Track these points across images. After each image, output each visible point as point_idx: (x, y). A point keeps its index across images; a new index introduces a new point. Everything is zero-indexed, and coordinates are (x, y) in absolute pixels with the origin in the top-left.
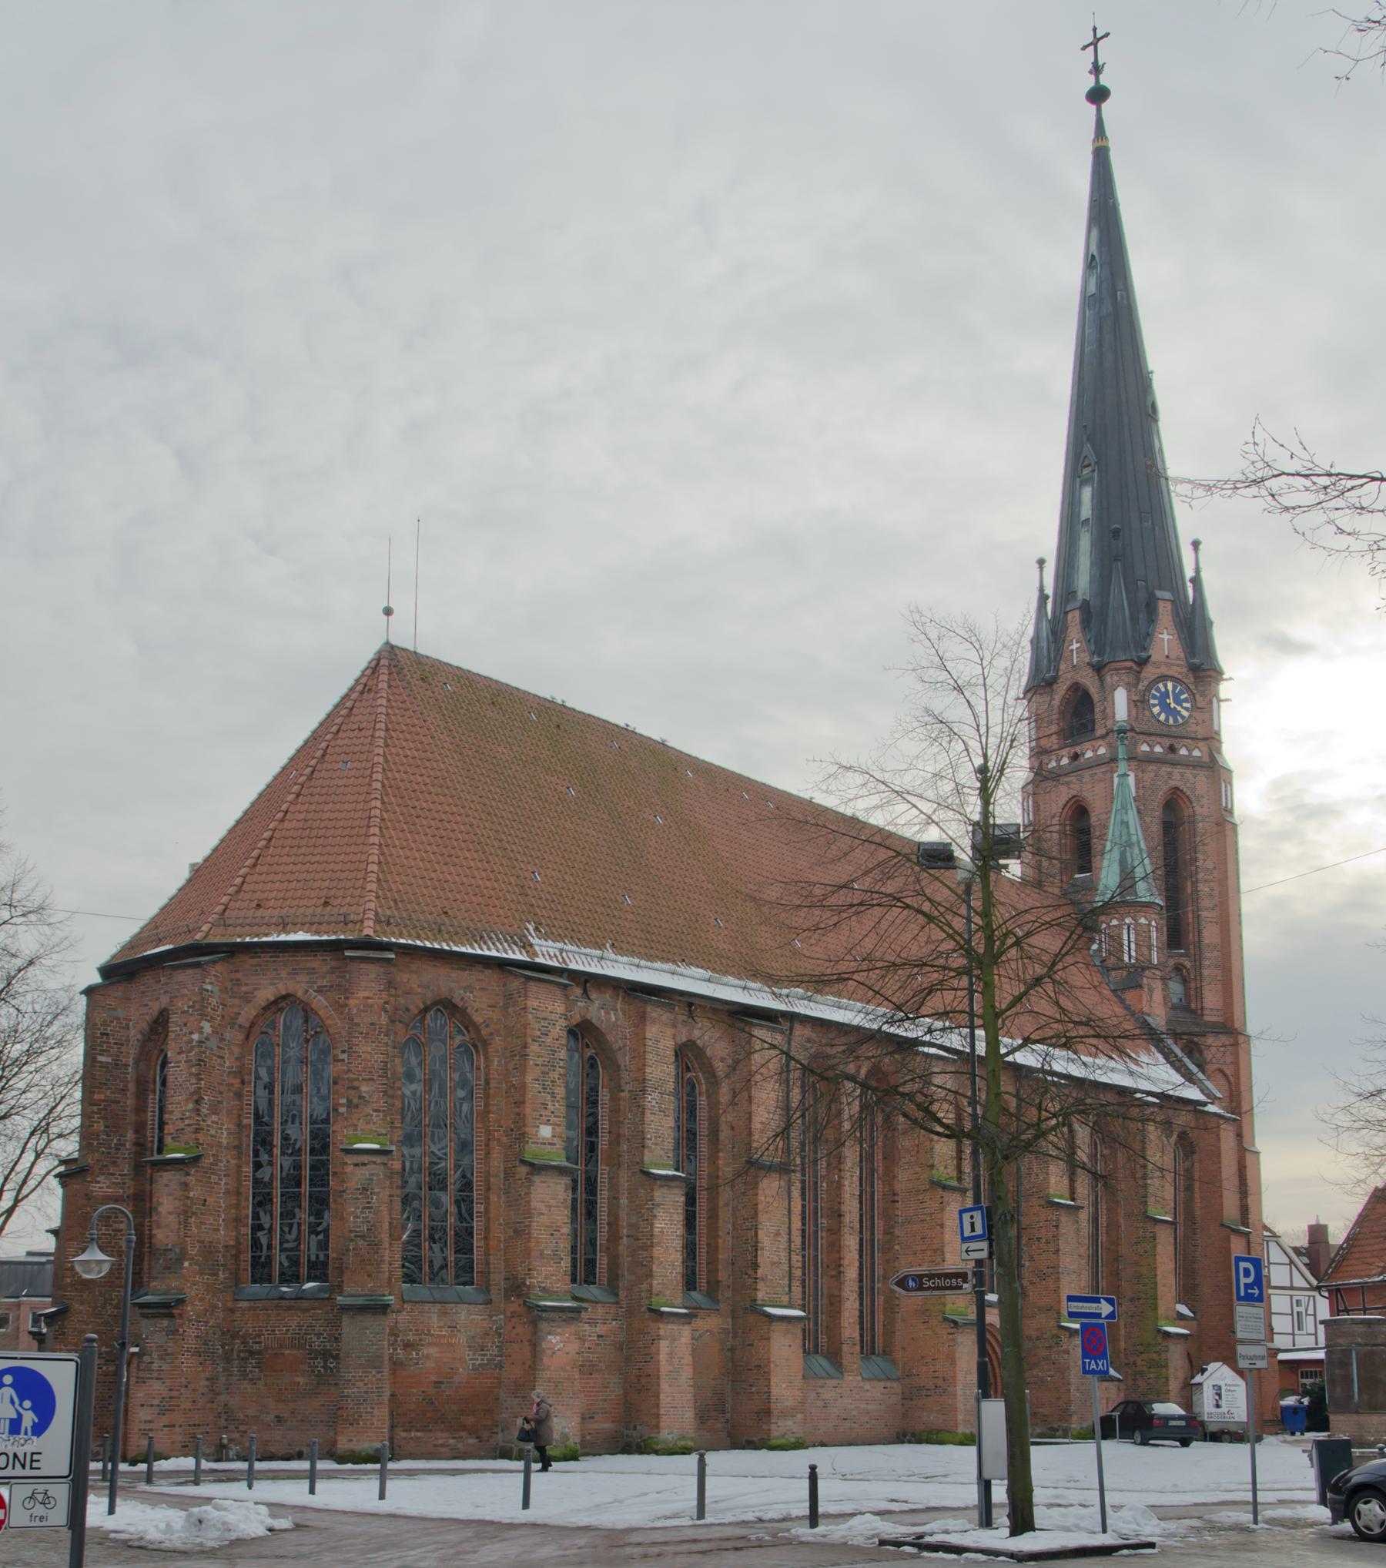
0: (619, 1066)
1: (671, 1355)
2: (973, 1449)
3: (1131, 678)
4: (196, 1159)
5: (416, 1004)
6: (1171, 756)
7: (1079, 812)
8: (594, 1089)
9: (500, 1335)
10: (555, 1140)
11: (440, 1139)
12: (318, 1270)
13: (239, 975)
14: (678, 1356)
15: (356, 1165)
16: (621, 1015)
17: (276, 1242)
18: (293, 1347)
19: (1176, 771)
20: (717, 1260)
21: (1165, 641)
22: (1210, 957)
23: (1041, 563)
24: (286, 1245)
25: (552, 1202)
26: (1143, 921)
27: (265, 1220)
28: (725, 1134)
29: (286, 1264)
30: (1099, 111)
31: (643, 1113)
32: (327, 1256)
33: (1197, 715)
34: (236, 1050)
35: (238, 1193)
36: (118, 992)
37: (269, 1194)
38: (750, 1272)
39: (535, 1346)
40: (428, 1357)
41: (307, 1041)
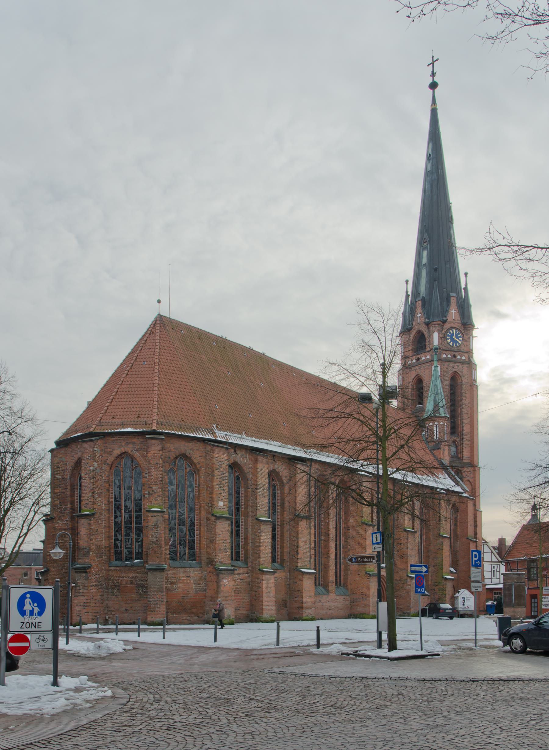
1: (267, 587)
2: (375, 621)
3: (440, 328)
4: (93, 514)
5: (173, 455)
6: (454, 359)
7: (419, 381)
8: (239, 488)
9: (205, 579)
10: (225, 507)
12: (139, 555)
14: (269, 586)
15: (152, 516)
17: (124, 545)
19: (456, 365)
21: (453, 313)
22: (466, 437)
23: (407, 282)
25: (224, 530)
26: (442, 423)
27: (119, 537)
29: (127, 553)
33: (465, 343)
34: (107, 473)
36: (62, 451)
37: (120, 527)
38: (296, 556)
40: (179, 587)
41: (133, 470)
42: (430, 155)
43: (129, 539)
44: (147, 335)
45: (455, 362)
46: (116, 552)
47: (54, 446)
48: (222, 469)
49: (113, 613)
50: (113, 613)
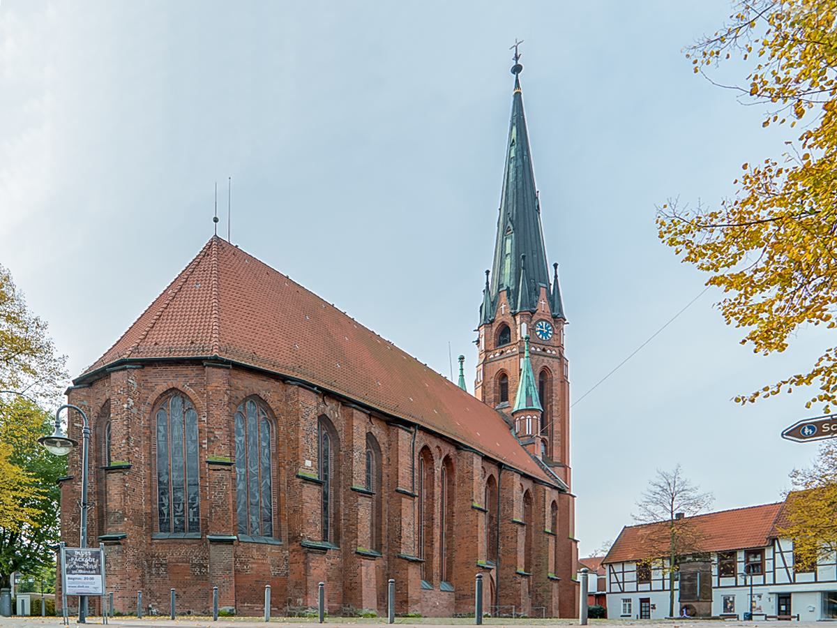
0: (339, 439)
1: (367, 574)
2: (813, 574)
3: (529, 319)
4: (129, 467)
5: (241, 395)
6: (543, 353)
7: (503, 375)
8: (326, 450)
9: (287, 560)
10: (313, 468)
11: (254, 466)
12: (194, 526)
13: (147, 378)
14: (369, 572)
15: (214, 470)
16: (340, 415)
17: (172, 511)
18: (183, 562)
19: (546, 359)
20: (381, 535)
21: (543, 305)
22: (556, 436)
23: (488, 272)
24: (177, 514)
25: (312, 497)
26: (535, 417)
27: (165, 501)
28: (385, 478)
29: (177, 523)
30: (517, 62)
31: (352, 461)
32: (198, 519)
33: (555, 337)
34: (147, 416)
35: (151, 487)
36: (84, 392)
37: (168, 489)
38: (397, 540)
39: (306, 564)
40: (252, 568)
41: (184, 413)
42: (513, 141)
43: (179, 504)
44: (200, 257)
45: (545, 356)
46: (161, 522)
47: (72, 385)
48: (309, 418)
49: (158, 600)
50: (158, 600)
